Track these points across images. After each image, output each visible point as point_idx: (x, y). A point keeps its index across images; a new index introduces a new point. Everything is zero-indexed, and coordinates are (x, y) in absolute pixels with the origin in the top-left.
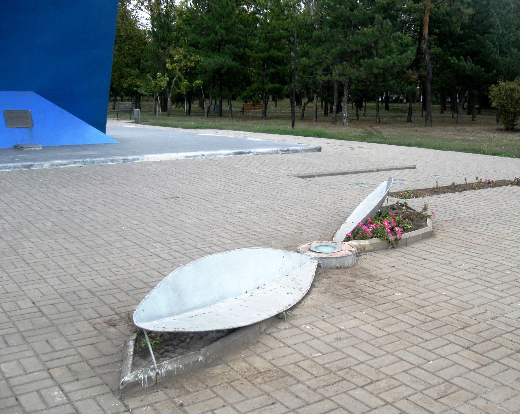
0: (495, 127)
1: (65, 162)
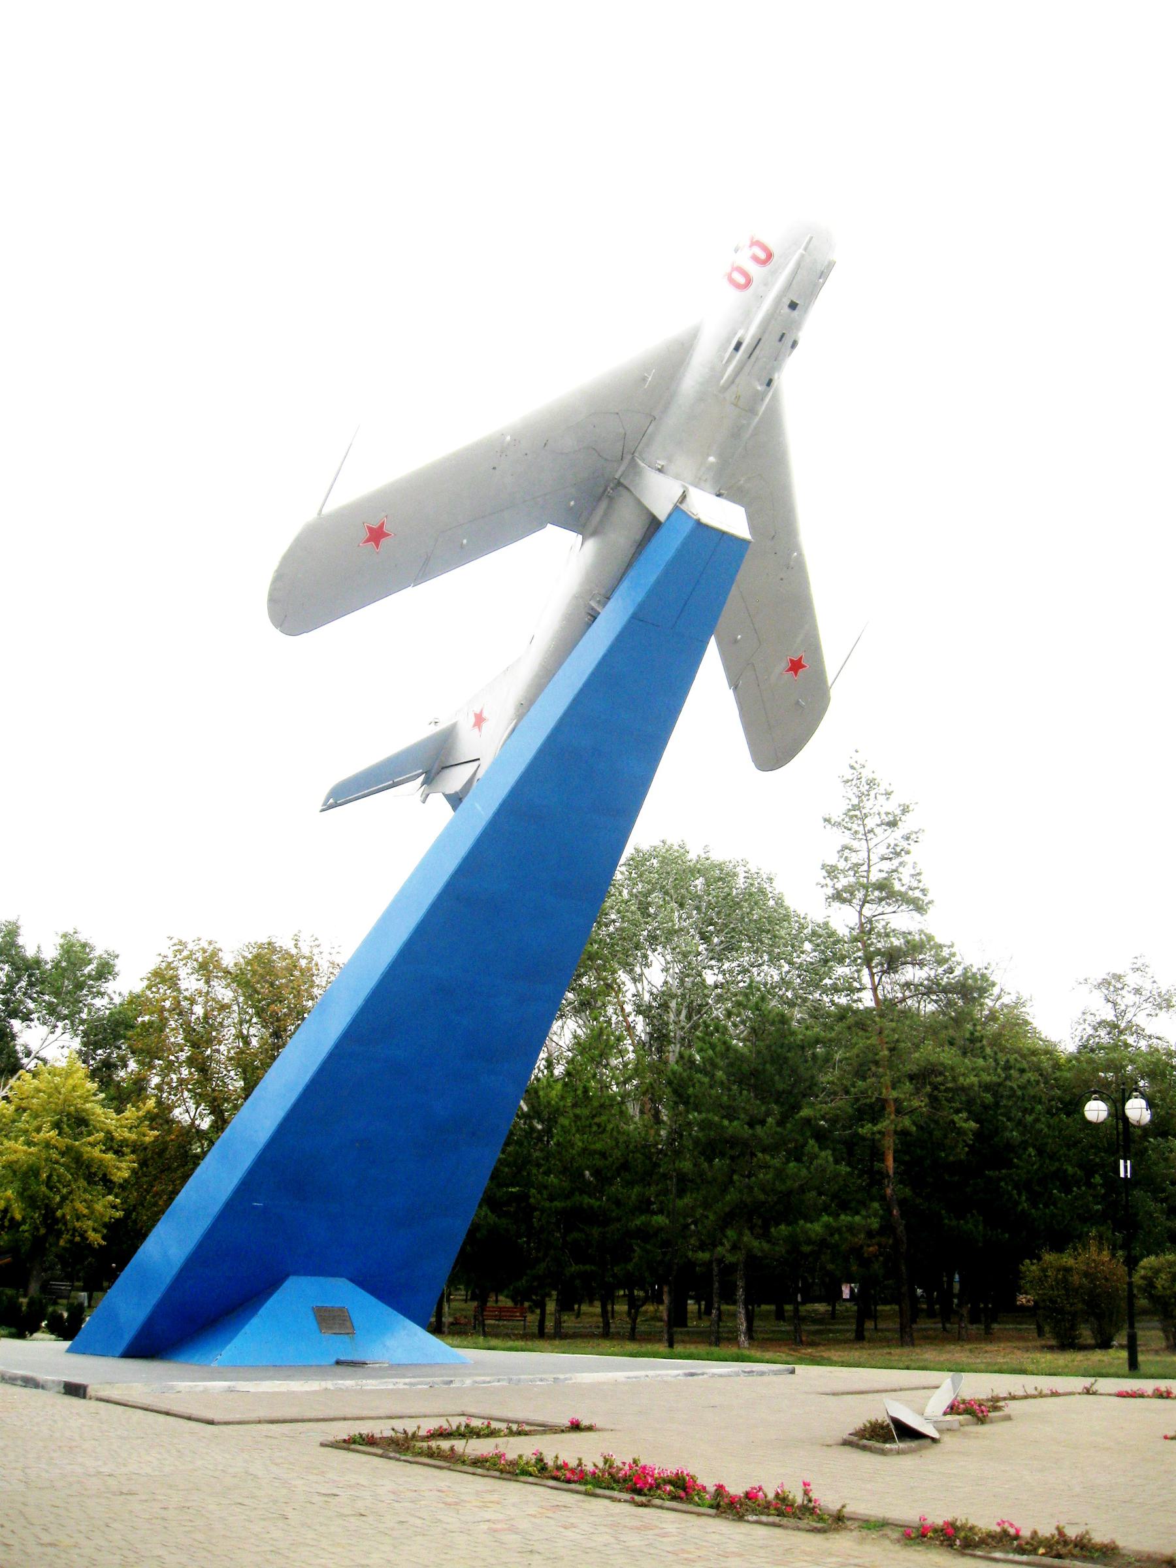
0: (1038, 1343)
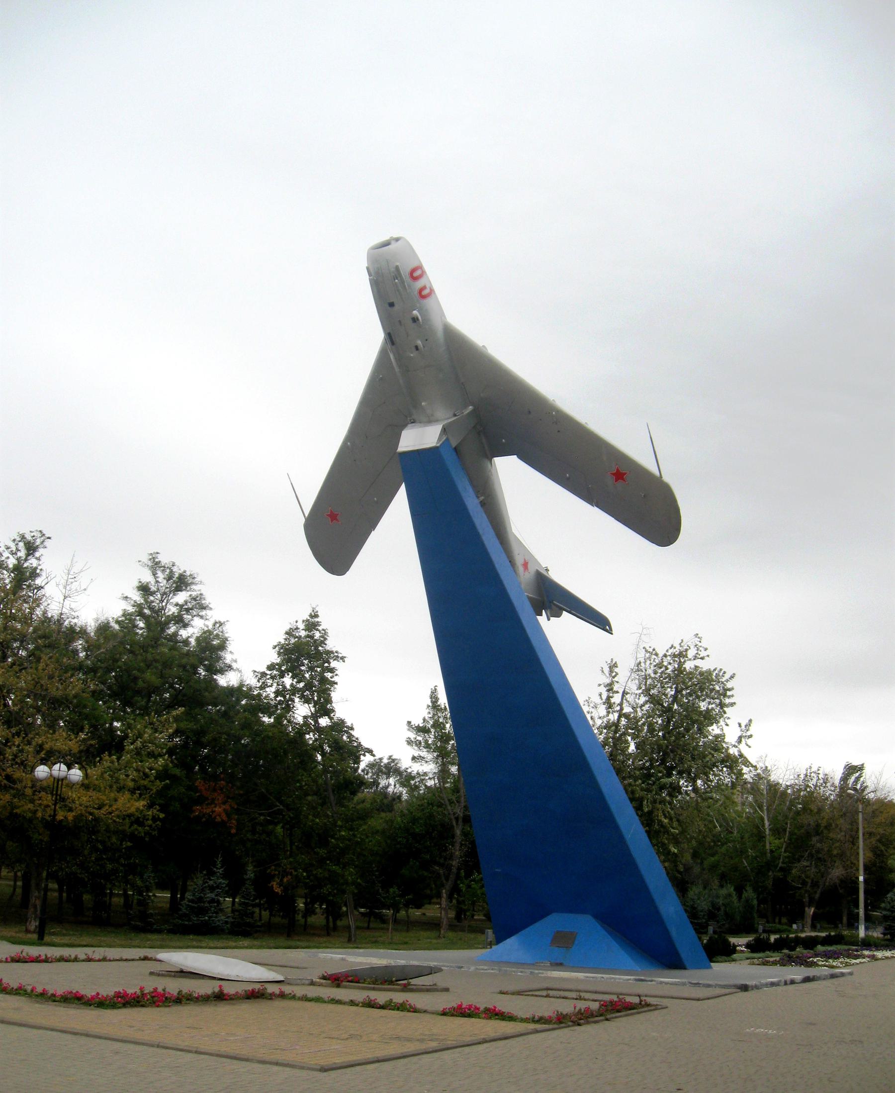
1: (486, 968)
